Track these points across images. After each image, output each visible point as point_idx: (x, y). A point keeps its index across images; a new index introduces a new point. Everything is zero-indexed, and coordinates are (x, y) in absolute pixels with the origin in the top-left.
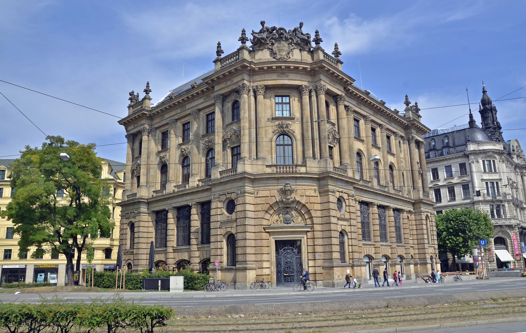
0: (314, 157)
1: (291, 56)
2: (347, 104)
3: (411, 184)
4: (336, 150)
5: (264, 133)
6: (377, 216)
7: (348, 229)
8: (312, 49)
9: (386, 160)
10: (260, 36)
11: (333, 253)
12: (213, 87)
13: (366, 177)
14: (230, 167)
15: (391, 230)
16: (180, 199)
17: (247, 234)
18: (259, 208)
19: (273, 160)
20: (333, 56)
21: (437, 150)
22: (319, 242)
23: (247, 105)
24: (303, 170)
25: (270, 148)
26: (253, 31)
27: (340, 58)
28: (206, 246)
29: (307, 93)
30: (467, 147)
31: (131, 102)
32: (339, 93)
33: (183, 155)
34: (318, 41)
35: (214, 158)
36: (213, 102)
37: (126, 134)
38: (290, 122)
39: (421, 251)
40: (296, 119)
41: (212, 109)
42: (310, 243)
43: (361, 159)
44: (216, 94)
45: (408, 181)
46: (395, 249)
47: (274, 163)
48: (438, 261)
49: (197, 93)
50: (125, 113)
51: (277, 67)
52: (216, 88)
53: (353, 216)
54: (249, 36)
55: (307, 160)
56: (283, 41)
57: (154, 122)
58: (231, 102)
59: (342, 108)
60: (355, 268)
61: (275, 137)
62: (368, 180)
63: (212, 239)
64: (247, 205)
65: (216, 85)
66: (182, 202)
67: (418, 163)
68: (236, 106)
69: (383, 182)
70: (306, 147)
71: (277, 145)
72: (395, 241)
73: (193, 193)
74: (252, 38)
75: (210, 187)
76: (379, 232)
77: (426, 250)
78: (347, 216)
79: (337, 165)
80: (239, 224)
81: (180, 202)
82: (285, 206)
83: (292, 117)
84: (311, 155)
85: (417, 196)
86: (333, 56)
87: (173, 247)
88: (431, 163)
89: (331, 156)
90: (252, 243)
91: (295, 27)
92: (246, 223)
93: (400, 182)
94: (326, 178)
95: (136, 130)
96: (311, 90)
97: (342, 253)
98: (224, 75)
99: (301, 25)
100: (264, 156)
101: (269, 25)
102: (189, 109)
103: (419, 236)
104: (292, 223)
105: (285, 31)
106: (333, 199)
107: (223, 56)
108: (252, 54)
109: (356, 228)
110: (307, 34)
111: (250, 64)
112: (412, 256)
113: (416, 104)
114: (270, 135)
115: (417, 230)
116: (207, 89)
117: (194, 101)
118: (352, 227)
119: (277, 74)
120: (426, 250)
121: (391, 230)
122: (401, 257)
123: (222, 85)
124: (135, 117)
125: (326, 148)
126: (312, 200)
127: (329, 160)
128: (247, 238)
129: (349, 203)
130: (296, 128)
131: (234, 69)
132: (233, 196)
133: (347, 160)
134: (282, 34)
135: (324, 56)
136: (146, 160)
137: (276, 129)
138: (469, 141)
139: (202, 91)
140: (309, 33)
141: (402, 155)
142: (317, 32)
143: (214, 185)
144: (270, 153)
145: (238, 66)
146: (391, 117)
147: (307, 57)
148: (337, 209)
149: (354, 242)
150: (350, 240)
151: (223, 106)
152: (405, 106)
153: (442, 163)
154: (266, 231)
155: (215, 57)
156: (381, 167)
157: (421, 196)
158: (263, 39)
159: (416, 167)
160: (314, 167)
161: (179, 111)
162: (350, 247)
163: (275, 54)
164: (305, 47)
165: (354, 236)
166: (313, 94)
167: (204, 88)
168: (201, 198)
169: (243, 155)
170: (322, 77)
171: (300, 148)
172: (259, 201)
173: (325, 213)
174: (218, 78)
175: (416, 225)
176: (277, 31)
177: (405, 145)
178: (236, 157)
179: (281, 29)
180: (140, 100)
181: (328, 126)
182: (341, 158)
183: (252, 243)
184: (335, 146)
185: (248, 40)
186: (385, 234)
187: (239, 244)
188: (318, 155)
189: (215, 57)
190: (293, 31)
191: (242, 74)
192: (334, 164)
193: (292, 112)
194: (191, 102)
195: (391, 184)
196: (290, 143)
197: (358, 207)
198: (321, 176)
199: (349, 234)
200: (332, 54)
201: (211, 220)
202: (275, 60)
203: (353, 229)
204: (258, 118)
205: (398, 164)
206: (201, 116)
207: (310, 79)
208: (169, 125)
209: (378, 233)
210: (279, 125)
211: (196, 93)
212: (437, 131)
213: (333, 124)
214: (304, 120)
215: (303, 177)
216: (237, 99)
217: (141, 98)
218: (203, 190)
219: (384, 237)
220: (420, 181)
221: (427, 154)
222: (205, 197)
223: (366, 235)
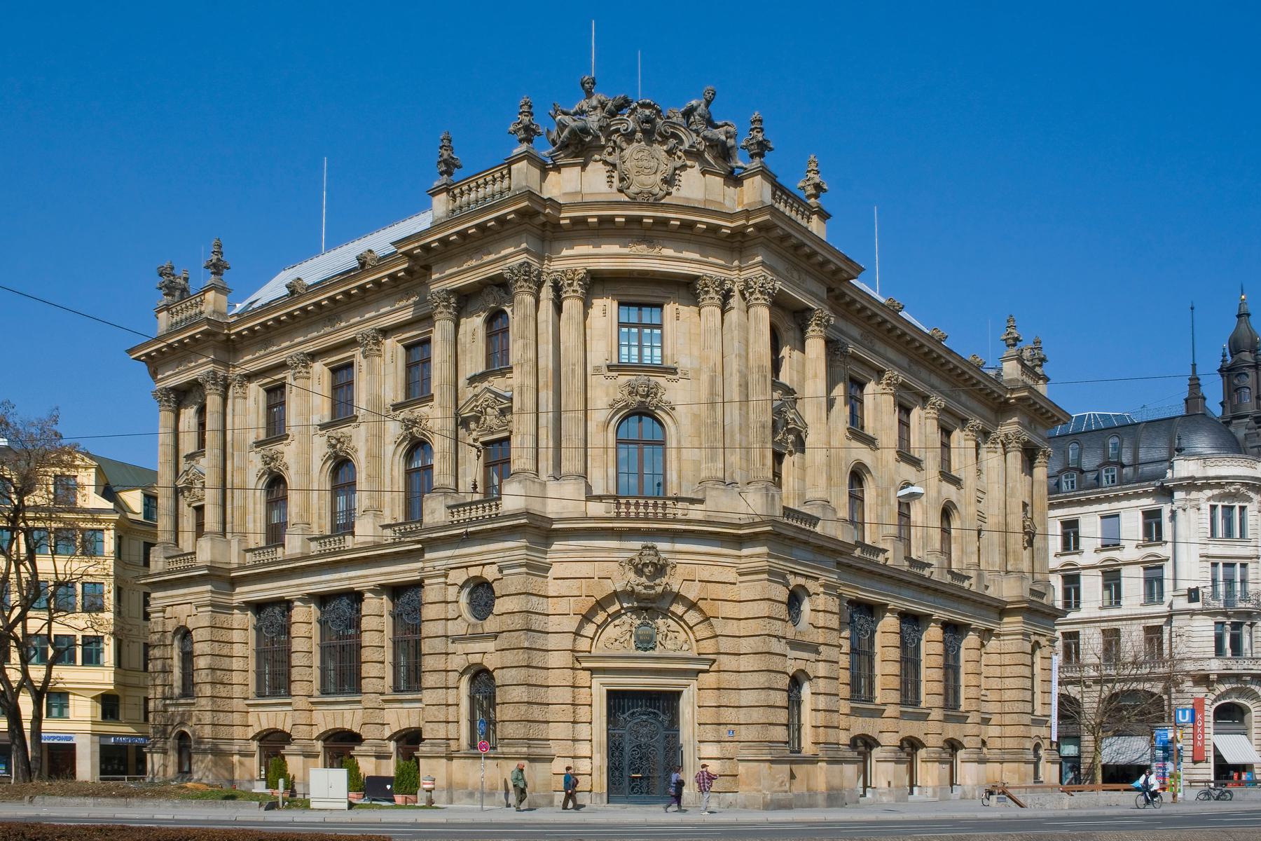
38: (661, 381)
51: (630, 220)
96: (730, 290)
130: (674, 392)
135: (774, 195)
153: (1134, 502)
154: (585, 665)
166: (735, 301)
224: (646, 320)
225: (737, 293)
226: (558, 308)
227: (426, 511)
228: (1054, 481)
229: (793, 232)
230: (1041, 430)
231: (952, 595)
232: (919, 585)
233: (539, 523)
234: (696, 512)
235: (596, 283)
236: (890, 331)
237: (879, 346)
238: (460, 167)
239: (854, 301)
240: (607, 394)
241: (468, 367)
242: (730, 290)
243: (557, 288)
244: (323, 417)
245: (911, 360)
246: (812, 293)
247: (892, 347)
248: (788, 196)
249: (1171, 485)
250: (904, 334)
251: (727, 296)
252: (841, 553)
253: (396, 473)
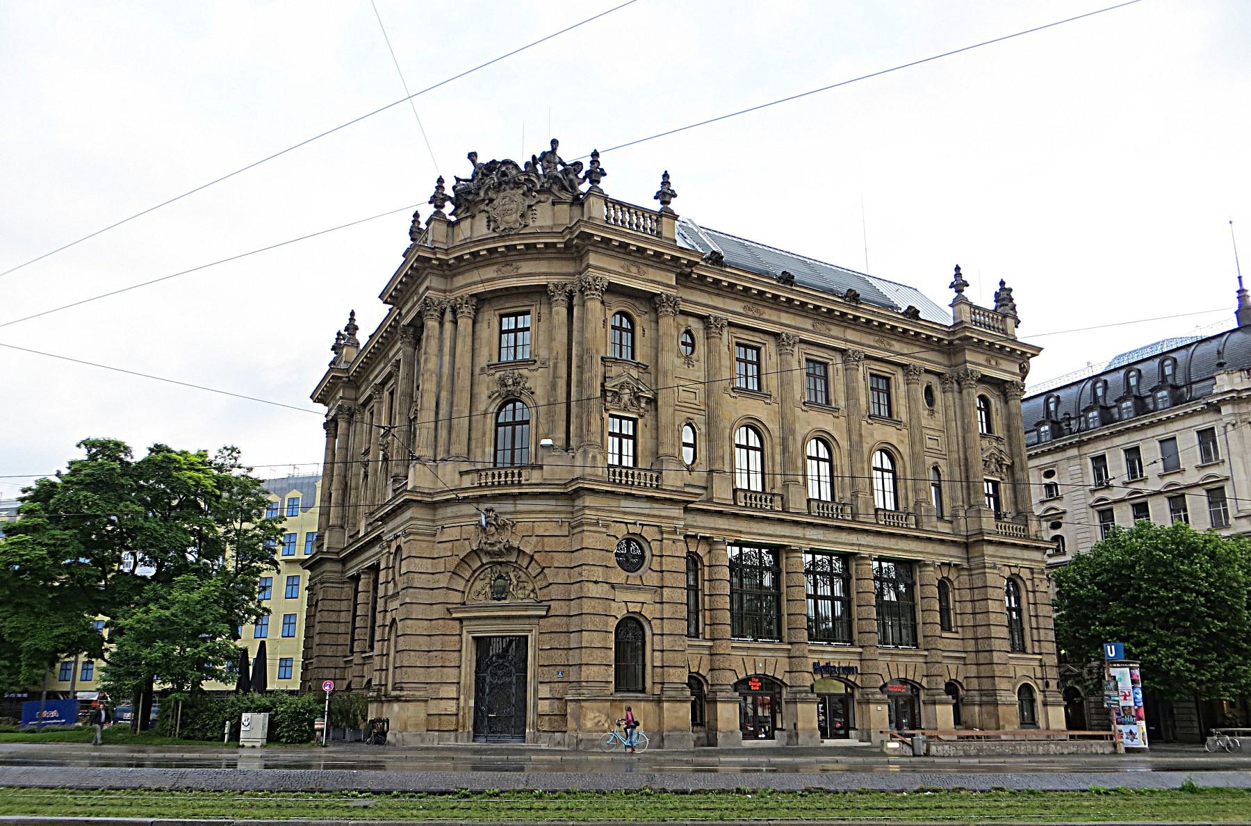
38: (525, 372)
60: (665, 705)
61: (493, 408)
82: (497, 562)
96: (571, 292)
101: (483, 159)
105: (516, 166)
111: (435, 254)
115: (974, 613)
119: (495, 268)
126: (550, 544)
130: (536, 381)
149: (668, 642)
153: (1150, 433)
154: (454, 615)
162: (657, 654)
166: (448, 316)
177: (949, 395)
203: (668, 611)
215: (526, 494)
225: (577, 294)
226: (455, 322)
234: (536, 476)
235: (481, 301)
238: (675, 196)
242: (571, 292)
243: (454, 312)
249: (1214, 400)
251: (570, 297)
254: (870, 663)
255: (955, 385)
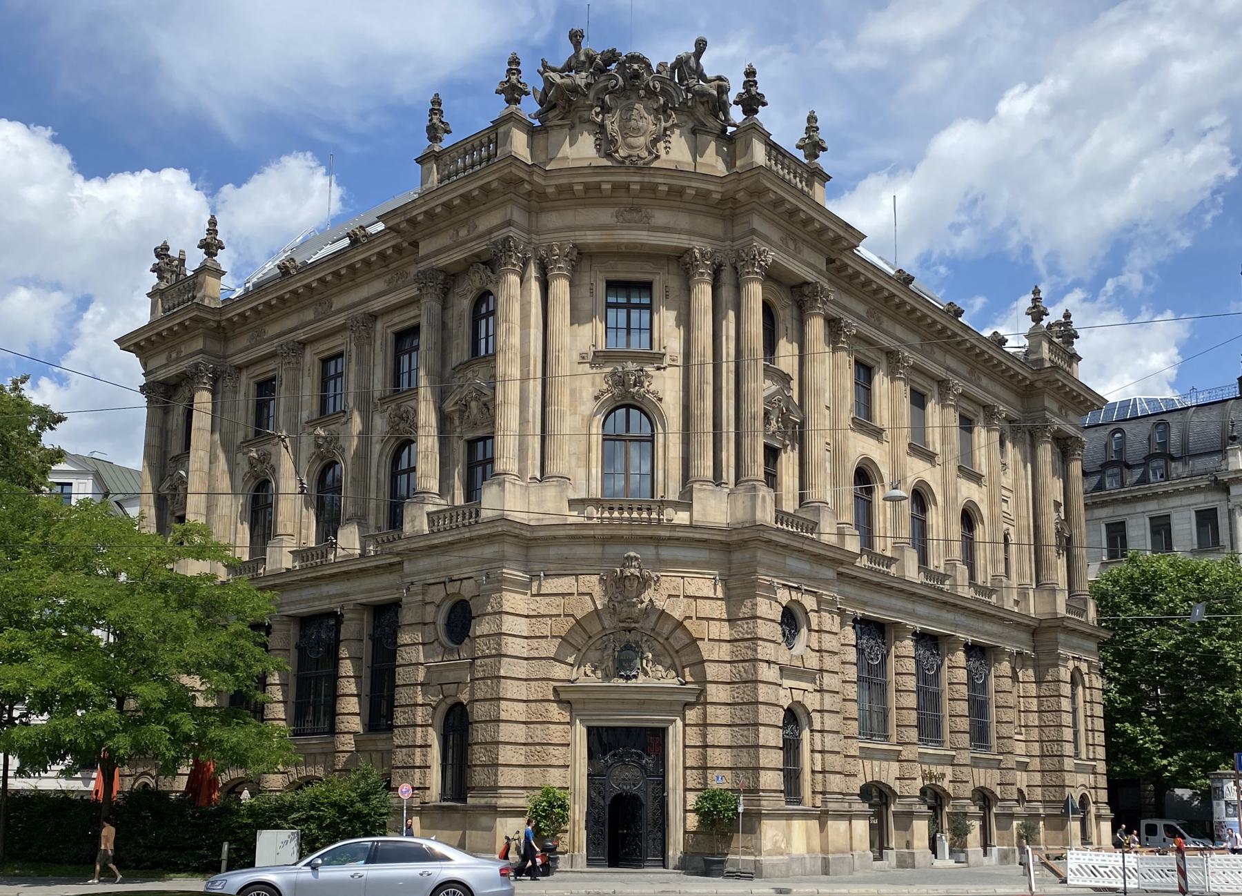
0: (717, 478)
1: (662, 152)
2: (835, 312)
3: (1029, 568)
4: (788, 463)
5: (566, 399)
6: (911, 666)
7: (812, 701)
8: (730, 129)
9: (951, 493)
10: (568, 81)
11: (762, 773)
12: (415, 244)
13: (883, 546)
14: (459, 500)
15: (955, 708)
16: (307, 593)
17: (504, 704)
18: (545, 628)
19: (593, 484)
20: (800, 155)
21: (1129, 467)
22: (720, 736)
23: (516, 307)
24: (682, 517)
25: (584, 448)
26: (545, 66)
27: (823, 161)
28: (384, 736)
29: (706, 272)
30: (1225, 458)
31: (160, 278)
32: (810, 276)
33: (321, 457)
34: (751, 102)
35: (414, 469)
36: (412, 292)
37: (143, 380)
39: (1052, 779)
40: (667, 360)
41: (412, 314)
42: (694, 738)
43: (870, 491)
44: (423, 266)
45: (1020, 561)
46: (964, 769)
47: (596, 492)
48: (1106, 811)
49: (366, 262)
50: (141, 315)
51: (616, 187)
52: (425, 248)
53: (829, 662)
54: (532, 80)
55: (696, 486)
56: (640, 99)
57: (232, 348)
58: (470, 297)
59: (816, 327)
62: (889, 554)
63: (400, 718)
64: (505, 617)
65: (423, 238)
66: (314, 599)
67: (1057, 504)
68: (484, 310)
69: (936, 562)
70: (695, 448)
71: (606, 438)
72: (967, 744)
73: (347, 575)
74: (540, 86)
75: (398, 559)
76: (914, 714)
77: (1067, 776)
78: (813, 662)
79: (790, 505)
80: (481, 675)
81: (308, 600)
83: (656, 350)
84: (709, 474)
85: (1048, 609)
86: (800, 155)
87: (354, 733)
88: (1104, 504)
89: (771, 479)
90: (520, 733)
91: (682, 53)
92: (502, 673)
93: (994, 563)
94: (752, 545)
95: (173, 370)
97: (792, 776)
98: (447, 206)
99: (701, 46)
100: (565, 474)
101: (594, 45)
102: (340, 311)
103: (1046, 730)
104: (641, 678)
106: (769, 609)
107: (447, 141)
108: (540, 140)
109: (838, 698)
110: (720, 78)
112: (1020, 791)
113: (1067, 316)
114: (588, 406)
115: (1040, 712)
116: (397, 249)
117: (357, 286)
118: (827, 696)
119: (613, 210)
120: (1067, 776)
121: (955, 708)
122: (984, 798)
123: (443, 240)
124: (170, 329)
125: (754, 451)
127: (764, 491)
128: (503, 716)
129: (820, 623)
130: (666, 386)
131: (481, 187)
132: (467, 589)
133: (822, 490)
134: (636, 75)
135: (769, 155)
136: (206, 468)
137: (605, 386)
138: (1234, 438)
139: (381, 255)
140: (724, 75)
141: (1007, 480)
142: (750, 73)
143: (413, 553)
144: (583, 463)
145: (491, 178)
146: (984, 357)
147: (713, 162)
148: (780, 639)
149: (830, 742)
150: (818, 735)
151: (444, 308)
152: (1028, 323)
153: (1140, 507)
155: (424, 144)
156: (934, 517)
157: (1062, 610)
158: (574, 89)
159: (1051, 519)
160: (714, 509)
161: (309, 315)
162: (818, 756)
163: (613, 141)
164: (711, 123)
165: (831, 722)
166: (726, 276)
167: (387, 246)
168: (371, 591)
169: (500, 466)
170: (758, 223)
171: (675, 450)
172: (542, 606)
173: (743, 651)
174: (430, 214)
175: (1038, 697)
176: (622, 64)
178: (480, 469)
179: (634, 58)
180: (189, 273)
181: (770, 387)
182: (802, 486)
183: (520, 733)
184: (785, 446)
185: (527, 94)
186: (938, 724)
187: (480, 734)
188: (729, 474)
189: (423, 144)
190: (673, 68)
191: (503, 204)
192: (778, 501)
193: (656, 335)
194: (348, 289)
195: (962, 571)
196: (647, 431)
197: (850, 635)
198: (735, 538)
199: (816, 717)
200: (799, 147)
201: (399, 661)
202: (606, 162)
203: (829, 701)
204: (550, 347)
205: (992, 504)
206: (378, 336)
207: (717, 228)
208: (279, 360)
209: (912, 718)
210: (613, 374)
211: (363, 260)
212: (1135, 405)
213: (785, 379)
214: (695, 361)
216: (490, 287)
217: (191, 267)
218: (377, 567)
219: (929, 728)
220: (1062, 563)
221: (1095, 480)
222: (385, 589)
223: (874, 723)
224: (634, 300)
227: (406, 519)
228: (1095, 480)
229: (786, 196)
230: (1072, 417)
231: (975, 611)
232: (935, 600)
233: (517, 531)
236: (898, 306)
237: (887, 324)
239: (857, 274)
240: (593, 385)
241: (454, 355)
244: (311, 413)
245: (924, 339)
246: (810, 265)
247: (901, 324)
248: (784, 156)
249: (1226, 478)
250: (914, 310)
252: (841, 563)
253: (382, 476)
254: (742, 742)
255: (1028, 437)
